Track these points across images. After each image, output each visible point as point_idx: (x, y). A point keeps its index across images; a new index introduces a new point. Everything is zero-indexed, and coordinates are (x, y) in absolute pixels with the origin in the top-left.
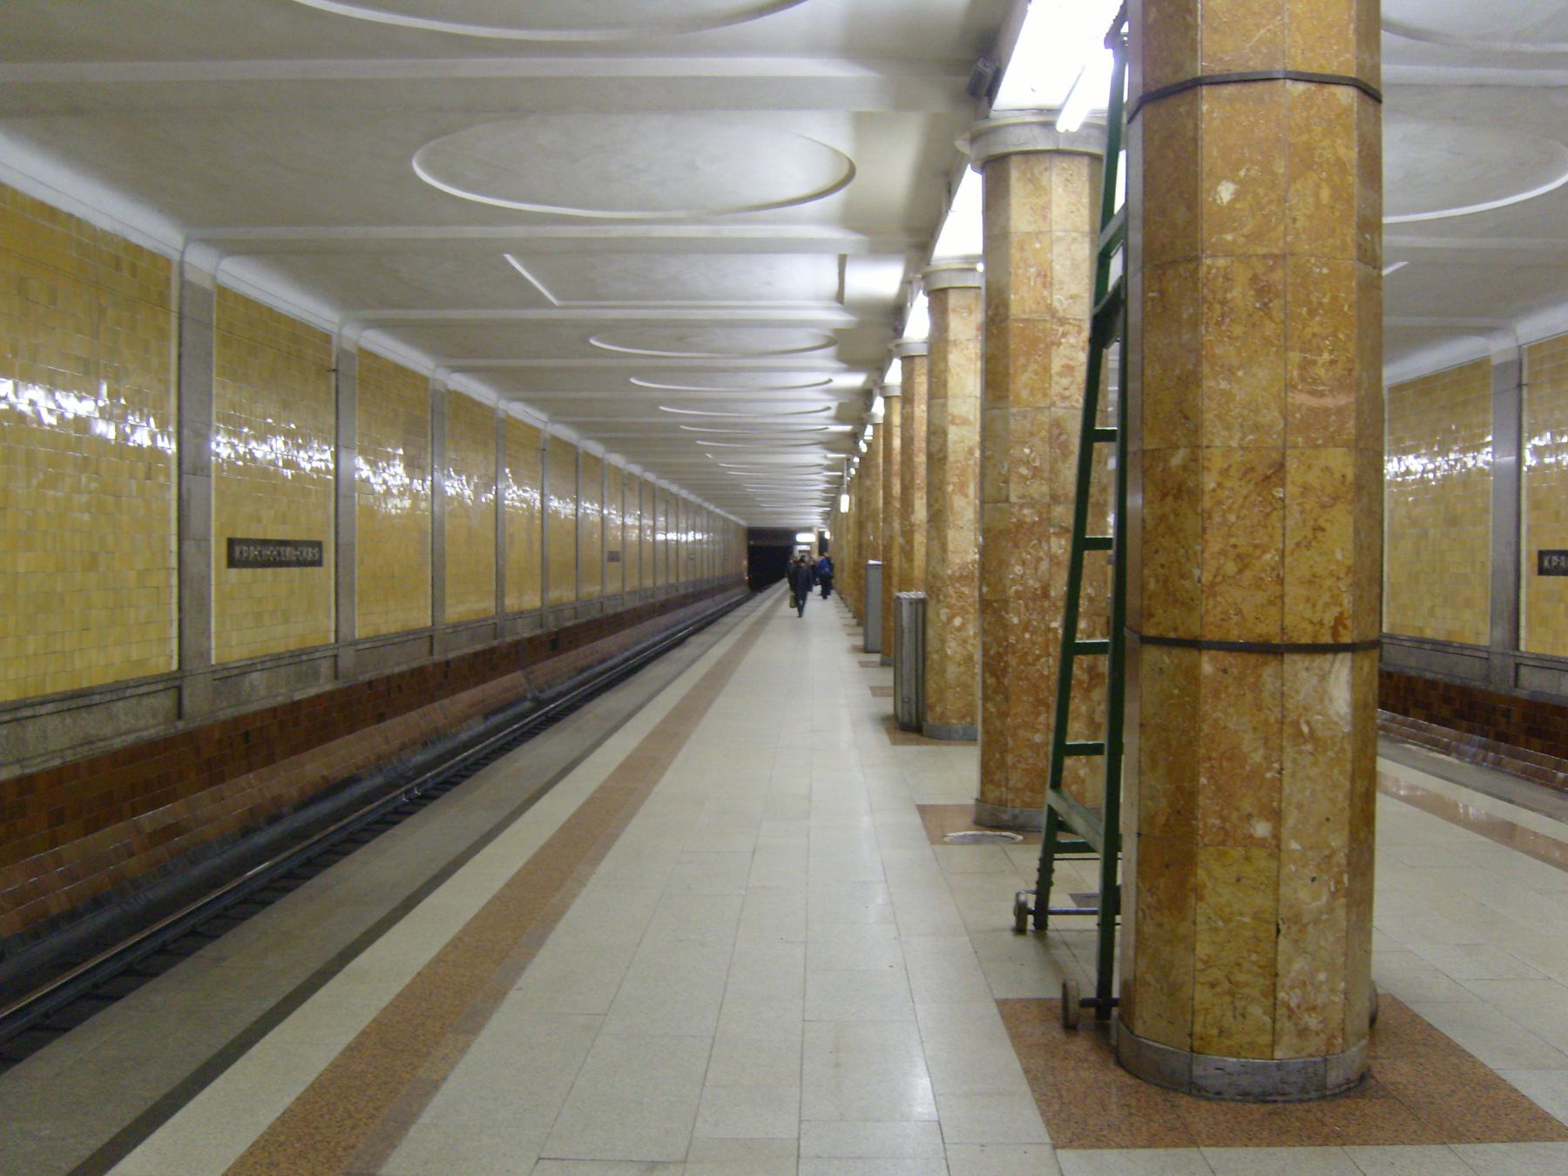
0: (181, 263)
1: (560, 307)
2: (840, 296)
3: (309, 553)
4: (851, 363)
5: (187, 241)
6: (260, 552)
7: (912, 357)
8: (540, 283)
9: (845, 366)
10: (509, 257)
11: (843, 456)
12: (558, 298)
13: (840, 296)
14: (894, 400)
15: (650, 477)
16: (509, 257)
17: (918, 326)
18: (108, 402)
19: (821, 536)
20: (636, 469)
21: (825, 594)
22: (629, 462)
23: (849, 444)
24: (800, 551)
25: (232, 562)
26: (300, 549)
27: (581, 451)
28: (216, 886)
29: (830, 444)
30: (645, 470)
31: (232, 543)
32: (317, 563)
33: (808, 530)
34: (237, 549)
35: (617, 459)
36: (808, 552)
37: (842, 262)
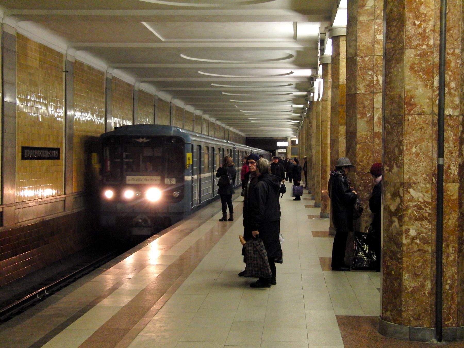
0: (66, 54)
1: (165, 42)
2: (295, 37)
3: (54, 153)
4: (301, 65)
5: (68, 47)
6: (34, 153)
7: (338, 37)
8: (156, 31)
9: (297, 90)
10: (144, 23)
11: (299, 115)
12: (164, 36)
13: (295, 37)
14: (342, 39)
15: (227, 127)
16: (144, 23)
17: (329, 50)
18: (381, 131)
19: (293, 142)
20: (223, 125)
21: (297, 196)
22: (186, 104)
23: (303, 100)
24: (280, 153)
25: (23, 158)
26: (50, 151)
27: (210, 122)
28: (53, 281)
29: (296, 100)
30: (230, 127)
31: (24, 149)
32: (58, 158)
33: (285, 139)
34: (26, 151)
35: (206, 117)
36: (286, 154)
37: (295, 24)
